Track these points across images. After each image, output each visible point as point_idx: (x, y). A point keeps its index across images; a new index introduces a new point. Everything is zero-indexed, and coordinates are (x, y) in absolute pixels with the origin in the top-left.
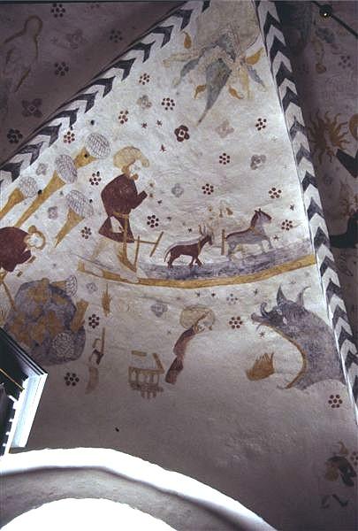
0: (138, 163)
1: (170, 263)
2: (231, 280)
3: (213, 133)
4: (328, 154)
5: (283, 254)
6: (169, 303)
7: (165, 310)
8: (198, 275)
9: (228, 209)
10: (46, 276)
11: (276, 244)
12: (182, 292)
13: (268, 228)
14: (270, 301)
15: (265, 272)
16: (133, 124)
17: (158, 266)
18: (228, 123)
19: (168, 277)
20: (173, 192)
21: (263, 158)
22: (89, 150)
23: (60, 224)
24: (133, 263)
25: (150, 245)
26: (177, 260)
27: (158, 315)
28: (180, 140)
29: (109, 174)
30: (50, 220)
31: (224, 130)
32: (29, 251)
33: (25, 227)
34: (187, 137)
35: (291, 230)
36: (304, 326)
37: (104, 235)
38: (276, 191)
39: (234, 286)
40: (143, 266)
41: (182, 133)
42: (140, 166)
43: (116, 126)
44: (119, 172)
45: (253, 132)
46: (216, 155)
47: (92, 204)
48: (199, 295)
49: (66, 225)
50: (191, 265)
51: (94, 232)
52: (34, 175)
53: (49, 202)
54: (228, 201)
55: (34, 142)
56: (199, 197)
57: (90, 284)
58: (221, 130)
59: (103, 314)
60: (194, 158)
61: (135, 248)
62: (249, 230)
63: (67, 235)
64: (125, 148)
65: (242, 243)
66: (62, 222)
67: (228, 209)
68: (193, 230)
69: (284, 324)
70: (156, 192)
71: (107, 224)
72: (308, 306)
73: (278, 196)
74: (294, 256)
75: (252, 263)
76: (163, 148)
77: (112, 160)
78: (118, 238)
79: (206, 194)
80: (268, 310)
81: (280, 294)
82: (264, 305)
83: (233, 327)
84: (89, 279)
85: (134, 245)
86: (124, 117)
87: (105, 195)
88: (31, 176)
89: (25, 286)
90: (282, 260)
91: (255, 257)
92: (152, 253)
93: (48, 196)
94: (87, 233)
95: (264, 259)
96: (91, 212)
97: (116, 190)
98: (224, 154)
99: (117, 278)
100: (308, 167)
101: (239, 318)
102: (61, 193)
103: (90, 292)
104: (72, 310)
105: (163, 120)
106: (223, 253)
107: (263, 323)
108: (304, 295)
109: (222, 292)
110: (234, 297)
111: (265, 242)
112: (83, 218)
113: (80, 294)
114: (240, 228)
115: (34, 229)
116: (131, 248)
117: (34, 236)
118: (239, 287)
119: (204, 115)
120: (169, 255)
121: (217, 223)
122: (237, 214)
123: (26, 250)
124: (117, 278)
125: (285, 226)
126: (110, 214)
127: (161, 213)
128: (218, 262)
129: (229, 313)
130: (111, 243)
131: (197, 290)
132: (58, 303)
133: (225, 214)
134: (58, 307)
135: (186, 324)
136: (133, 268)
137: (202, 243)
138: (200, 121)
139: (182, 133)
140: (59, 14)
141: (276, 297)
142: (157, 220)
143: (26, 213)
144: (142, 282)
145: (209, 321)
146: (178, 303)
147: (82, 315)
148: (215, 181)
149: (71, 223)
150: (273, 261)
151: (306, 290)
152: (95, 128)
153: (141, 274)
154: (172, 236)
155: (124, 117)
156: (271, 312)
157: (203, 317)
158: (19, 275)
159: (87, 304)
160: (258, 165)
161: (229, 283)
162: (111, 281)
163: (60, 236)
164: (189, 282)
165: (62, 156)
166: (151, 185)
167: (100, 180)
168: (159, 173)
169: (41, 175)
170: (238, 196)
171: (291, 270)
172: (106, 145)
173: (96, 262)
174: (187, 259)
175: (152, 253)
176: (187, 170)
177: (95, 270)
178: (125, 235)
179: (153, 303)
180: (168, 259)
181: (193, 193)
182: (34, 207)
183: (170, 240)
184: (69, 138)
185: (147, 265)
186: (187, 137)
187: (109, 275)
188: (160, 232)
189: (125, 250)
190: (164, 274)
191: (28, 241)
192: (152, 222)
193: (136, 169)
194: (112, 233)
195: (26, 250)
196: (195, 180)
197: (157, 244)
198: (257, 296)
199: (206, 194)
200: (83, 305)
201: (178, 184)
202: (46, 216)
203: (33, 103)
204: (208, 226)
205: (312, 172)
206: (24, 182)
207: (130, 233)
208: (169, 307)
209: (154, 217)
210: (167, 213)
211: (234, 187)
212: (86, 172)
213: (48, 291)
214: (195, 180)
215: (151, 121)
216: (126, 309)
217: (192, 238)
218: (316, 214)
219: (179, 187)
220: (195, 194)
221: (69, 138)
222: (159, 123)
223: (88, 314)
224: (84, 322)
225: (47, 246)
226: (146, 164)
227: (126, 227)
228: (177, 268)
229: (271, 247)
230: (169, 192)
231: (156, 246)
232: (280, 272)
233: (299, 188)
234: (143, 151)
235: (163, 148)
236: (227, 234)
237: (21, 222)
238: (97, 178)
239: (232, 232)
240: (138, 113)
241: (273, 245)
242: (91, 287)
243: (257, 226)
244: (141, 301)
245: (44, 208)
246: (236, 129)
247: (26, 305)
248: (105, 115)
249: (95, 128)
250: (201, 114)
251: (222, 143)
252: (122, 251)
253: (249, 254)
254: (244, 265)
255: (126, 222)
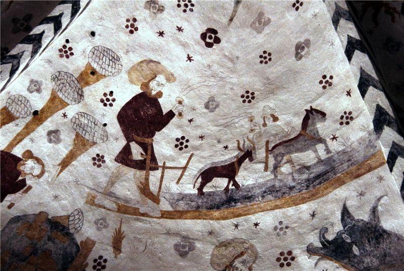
0: (161, 78)
1: (200, 189)
2: (278, 203)
3: (248, 30)
4: (386, 12)
5: (346, 158)
6: (197, 240)
7: (192, 248)
8: (236, 201)
9: (273, 116)
10: (44, 209)
11: (335, 146)
12: (215, 225)
13: (322, 128)
14: (332, 225)
15: (322, 186)
16: (146, 33)
17: (186, 195)
18: (263, 14)
19: (198, 207)
20: (207, 107)
21: (307, 43)
22: (95, 66)
23: (63, 150)
24: (155, 193)
25: (175, 171)
26: (209, 184)
27: (183, 255)
28: (209, 45)
29: (126, 92)
30: (51, 145)
31: (260, 24)
32: (24, 181)
33: (18, 151)
34: (217, 41)
35: (351, 123)
36: (385, 255)
37: (122, 162)
38: (328, 78)
39: (284, 210)
40: (167, 196)
41: (210, 38)
42: (164, 81)
43: (124, 37)
44: (137, 90)
45: (291, 15)
46: (255, 55)
47: (106, 127)
48: (236, 226)
49: (71, 151)
50: (227, 189)
51: (109, 161)
52: (25, 93)
53: (49, 124)
54: (271, 105)
55: (14, 52)
56: (239, 108)
57: (99, 220)
58: (257, 25)
59: (113, 255)
60: (230, 65)
61: (160, 175)
62: (300, 135)
63: (73, 163)
64: (141, 62)
65: (289, 153)
66: (66, 148)
67: (273, 116)
68: (230, 146)
69: (355, 255)
70: (185, 110)
71: (126, 150)
72: (387, 224)
73: (330, 85)
74: (359, 156)
75: (305, 176)
76: (189, 59)
77: (126, 76)
78: (140, 165)
79: (246, 103)
80: (330, 237)
81: (345, 212)
82: (324, 231)
83: (282, 265)
84: (99, 213)
85: (158, 173)
86: (132, 26)
87: (122, 117)
88: (22, 94)
89: (17, 219)
90: (345, 166)
91: (308, 168)
92: (179, 179)
93: (46, 118)
94: (99, 160)
95: (321, 169)
96: (106, 137)
97: (136, 111)
98: (265, 52)
99: (136, 212)
100: (350, 30)
101: (290, 253)
102: (65, 115)
103: (99, 229)
104: (74, 250)
105: (184, 25)
106: (266, 169)
107: (324, 257)
108: (380, 208)
109: (267, 219)
110: (283, 226)
111: (320, 148)
112: (95, 143)
113: (87, 231)
114: (289, 135)
115: (29, 155)
116: (154, 176)
117: (30, 163)
118: (291, 211)
119: (235, 11)
120: (200, 180)
121: (260, 135)
122: (283, 119)
123: (20, 178)
124: (136, 212)
125: (345, 120)
126: (129, 139)
127: (192, 133)
128: (261, 181)
129: (278, 247)
130: (131, 173)
131: (235, 221)
132: (57, 241)
133: (270, 123)
134: (55, 247)
135: (218, 265)
136: (156, 199)
137: (240, 161)
138: (231, 20)
139: (210, 37)
140: (267, 60)
141: (340, 218)
142: (187, 141)
143: (18, 135)
144: (165, 215)
145: (249, 259)
146: (209, 239)
147: (86, 256)
148: (256, 85)
149: (78, 149)
150: (333, 169)
151: (382, 201)
152: (97, 41)
153: (165, 206)
154: (203, 158)
155: (132, 26)
156: (336, 239)
157: (242, 254)
158: (10, 207)
159: (94, 243)
160: (303, 53)
161: (277, 207)
162: (126, 215)
163: (65, 164)
164: (224, 211)
165: (59, 72)
166: (180, 103)
167: (114, 100)
168: (188, 87)
169: (35, 94)
170: (283, 97)
171: (358, 176)
172: (115, 59)
173: (109, 194)
174: (220, 183)
175: (179, 179)
176: (222, 79)
177: (108, 203)
178: (148, 161)
179: (178, 240)
180: (198, 185)
181: (230, 105)
182: (28, 130)
183: (200, 162)
184: (66, 52)
185: (172, 194)
186: (217, 41)
187: (125, 209)
188: (189, 155)
189: (147, 179)
190: (193, 204)
191: (22, 168)
192: (181, 144)
193: (158, 85)
194: (132, 161)
195: (20, 178)
196: (232, 89)
197: (185, 169)
198: (315, 220)
199: (246, 103)
200: (89, 245)
201: (213, 97)
202: (45, 140)
203: (24, 19)
204: (249, 140)
205: (355, 34)
206: (13, 101)
207: (154, 159)
208: (198, 245)
209: (183, 138)
210: (199, 132)
211: (278, 88)
212: (92, 93)
213: (46, 226)
214: (232, 89)
215: (169, 29)
216: (142, 248)
217: (227, 157)
218: (371, 88)
219: (213, 100)
220: (233, 106)
221: (66, 52)
222: (180, 29)
223: (93, 255)
224: (87, 265)
225: (46, 174)
226: (170, 78)
227: (149, 152)
228: (210, 194)
229: (328, 151)
230: (201, 109)
231: (183, 172)
232: (343, 183)
233: (342, 55)
234: (164, 63)
235: (189, 59)
236: (271, 145)
237: (12, 145)
238: (111, 98)
239: (278, 142)
240: (149, 20)
241: (331, 149)
242: (101, 224)
243: (309, 129)
244: (162, 238)
245: (41, 131)
246: (273, 19)
247: (14, 241)
248: (106, 25)
249: (97, 41)
250: (230, 12)
251: (260, 39)
252: (143, 181)
253: (299, 165)
254: (294, 180)
255: (149, 148)
